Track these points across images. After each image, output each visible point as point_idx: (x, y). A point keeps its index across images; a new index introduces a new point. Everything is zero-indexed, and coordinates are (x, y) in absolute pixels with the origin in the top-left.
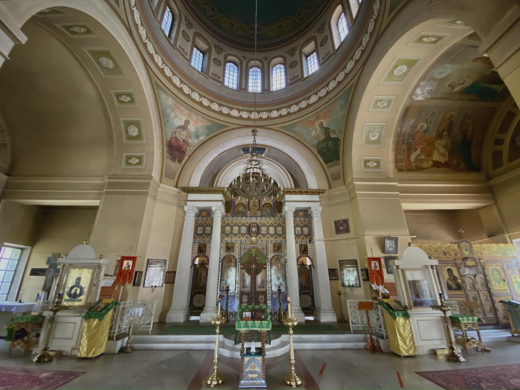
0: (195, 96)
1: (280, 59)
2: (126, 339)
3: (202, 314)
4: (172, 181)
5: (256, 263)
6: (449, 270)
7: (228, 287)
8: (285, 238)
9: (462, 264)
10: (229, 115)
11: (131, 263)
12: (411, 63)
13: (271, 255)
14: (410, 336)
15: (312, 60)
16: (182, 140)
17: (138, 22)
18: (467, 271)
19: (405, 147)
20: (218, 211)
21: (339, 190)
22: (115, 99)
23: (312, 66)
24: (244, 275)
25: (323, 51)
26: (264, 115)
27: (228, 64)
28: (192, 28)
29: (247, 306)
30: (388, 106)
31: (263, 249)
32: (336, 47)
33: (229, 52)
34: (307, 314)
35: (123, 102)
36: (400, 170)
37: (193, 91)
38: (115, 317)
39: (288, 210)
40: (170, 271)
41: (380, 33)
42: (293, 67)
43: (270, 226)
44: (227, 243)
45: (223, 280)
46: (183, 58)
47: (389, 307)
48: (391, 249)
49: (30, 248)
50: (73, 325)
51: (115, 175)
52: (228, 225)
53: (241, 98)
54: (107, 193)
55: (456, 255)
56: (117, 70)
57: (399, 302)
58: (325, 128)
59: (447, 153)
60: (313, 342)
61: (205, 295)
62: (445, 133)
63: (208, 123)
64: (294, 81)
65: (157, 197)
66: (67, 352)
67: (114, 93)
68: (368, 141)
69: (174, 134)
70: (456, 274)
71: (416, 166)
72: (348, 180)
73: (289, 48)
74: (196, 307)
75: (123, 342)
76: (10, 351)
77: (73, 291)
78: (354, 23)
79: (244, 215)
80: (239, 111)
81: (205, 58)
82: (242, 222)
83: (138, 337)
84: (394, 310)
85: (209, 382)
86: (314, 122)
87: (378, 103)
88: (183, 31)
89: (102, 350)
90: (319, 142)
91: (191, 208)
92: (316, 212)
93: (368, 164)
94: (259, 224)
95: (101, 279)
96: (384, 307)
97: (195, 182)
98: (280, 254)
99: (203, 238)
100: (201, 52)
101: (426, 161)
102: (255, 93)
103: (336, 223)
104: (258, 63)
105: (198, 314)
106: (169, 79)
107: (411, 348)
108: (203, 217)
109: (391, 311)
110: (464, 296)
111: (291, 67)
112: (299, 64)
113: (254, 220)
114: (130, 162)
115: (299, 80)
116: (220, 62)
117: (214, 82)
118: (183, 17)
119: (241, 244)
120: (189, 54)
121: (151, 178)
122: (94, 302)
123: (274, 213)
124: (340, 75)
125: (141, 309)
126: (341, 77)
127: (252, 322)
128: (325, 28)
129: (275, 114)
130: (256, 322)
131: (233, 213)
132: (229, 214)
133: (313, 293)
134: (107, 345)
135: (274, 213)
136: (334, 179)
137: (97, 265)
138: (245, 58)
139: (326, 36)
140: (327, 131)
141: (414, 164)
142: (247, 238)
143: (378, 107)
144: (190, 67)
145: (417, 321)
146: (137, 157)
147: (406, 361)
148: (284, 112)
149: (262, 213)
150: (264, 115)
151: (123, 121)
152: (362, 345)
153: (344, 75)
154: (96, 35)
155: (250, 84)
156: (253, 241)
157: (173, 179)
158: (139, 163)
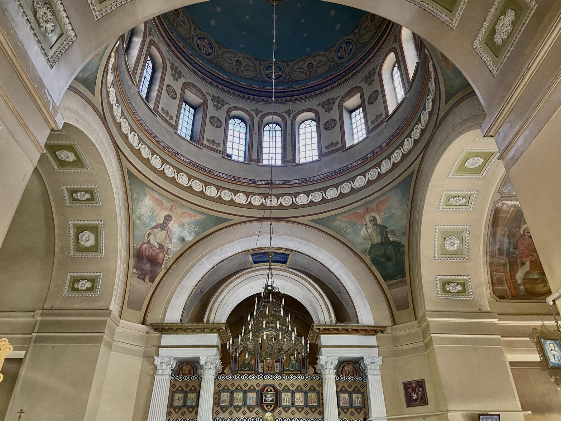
4: (138, 312)
8: (322, 413)
10: (232, 203)
12: (487, 157)
15: (358, 117)
16: (157, 246)
19: (504, 260)
21: (407, 328)
23: (357, 129)
25: (373, 110)
26: (287, 201)
27: (232, 121)
30: (467, 204)
32: (391, 111)
33: (234, 105)
35: (78, 200)
39: (326, 363)
42: (330, 127)
43: (297, 390)
46: (164, 124)
51: (51, 309)
56: (79, 163)
63: (199, 217)
64: (331, 149)
67: (67, 189)
68: (445, 253)
69: (146, 237)
71: (526, 290)
72: (420, 314)
73: (324, 98)
78: (411, 86)
79: (253, 371)
81: (197, 117)
86: (362, 216)
91: (166, 360)
97: (174, 315)
100: (191, 106)
101: (542, 283)
102: (272, 166)
103: (407, 386)
106: (147, 162)
108: (184, 375)
112: (338, 126)
115: (339, 149)
116: (221, 122)
117: (212, 153)
118: (168, 65)
120: (174, 119)
123: (304, 367)
124: (395, 154)
128: (374, 77)
129: (302, 200)
131: (235, 367)
135: (304, 367)
136: (399, 308)
140: (382, 229)
141: (522, 287)
144: (175, 135)
148: (317, 197)
149: (283, 366)
150: (287, 201)
151: (74, 225)
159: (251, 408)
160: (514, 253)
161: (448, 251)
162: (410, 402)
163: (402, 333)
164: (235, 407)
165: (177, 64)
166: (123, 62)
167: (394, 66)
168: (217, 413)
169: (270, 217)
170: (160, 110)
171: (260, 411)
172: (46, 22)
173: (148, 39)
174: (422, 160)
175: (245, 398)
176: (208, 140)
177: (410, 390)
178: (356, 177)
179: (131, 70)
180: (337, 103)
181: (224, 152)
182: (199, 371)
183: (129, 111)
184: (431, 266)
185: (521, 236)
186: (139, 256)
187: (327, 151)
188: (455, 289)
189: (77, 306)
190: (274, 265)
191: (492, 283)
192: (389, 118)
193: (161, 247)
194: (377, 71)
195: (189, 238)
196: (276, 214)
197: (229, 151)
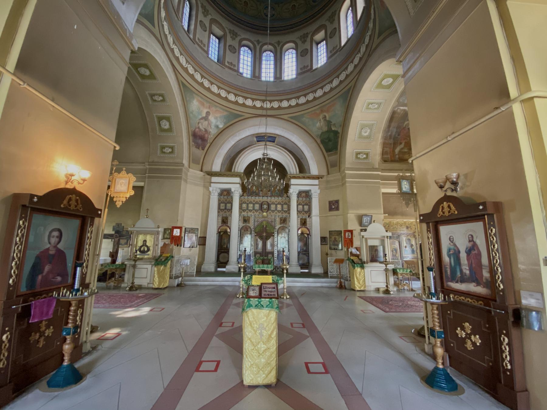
1: (292, 45)
2: (180, 279)
3: (227, 267)
5: (266, 232)
8: (289, 213)
10: (244, 105)
11: (179, 230)
19: (391, 141)
20: (236, 192)
22: (149, 98)
23: (321, 57)
24: (257, 240)
26: (276, 105)
27: (242, 49)
32: (343, 44)
33: (243, 37)
34: (302, 268)
36: (385, 161)
37: (212, 83)
42: (305, 54)
44: (244, 217)
48: (366, 224)
51: (153, 162)
52: (245, 203)
53: (254, 88)
56: (152, 76)
57: (361, 260)
61: (228, 254)
64: (304, 70)
65: (188, 180)
68: (361, 136)
71: (399, 158)
72: (342, 169)
77: (142, 249)
79: (257, 195)
80: (253, 100)
81: (220, 45)
82: (256, 200)
83: (186, 278)
88: (201, 21)
89: (167, 285)
90: (322, 133)
92: (315, 194)
93: (359, 156)
100: (217, 37)
103: (330, 203)
104: (270, 47)
105: (224, 267)
106: (192, 76)
115: (307, 71)
116: (235, 49)
117: (230, 71)
118: (200, 5)
120: (206, 46)
124: (342, 75)
125: (189, 261)
128: (335, 18)
129: (285, 104)
132: (245, 194)
134: (169, 281)
139: (335, 28)
141: (397, 156)
142: (260, 213)
144: (208, 59)
150: (276, 105)
151: (156, 116)
152: (334, 285)
157: (199, 164)
159: (256, 211)
167: (349, 9)
168: (241, 212)
169: (265, 114)
170: (197, 40)
175: (254, 207)
180: (310, 36)
181: (238, 71)
183: (178, 40)
184: (352, 144)
189: (166, 161)
190: (268, 143)
195: (221, 126)
196: (270, 113)
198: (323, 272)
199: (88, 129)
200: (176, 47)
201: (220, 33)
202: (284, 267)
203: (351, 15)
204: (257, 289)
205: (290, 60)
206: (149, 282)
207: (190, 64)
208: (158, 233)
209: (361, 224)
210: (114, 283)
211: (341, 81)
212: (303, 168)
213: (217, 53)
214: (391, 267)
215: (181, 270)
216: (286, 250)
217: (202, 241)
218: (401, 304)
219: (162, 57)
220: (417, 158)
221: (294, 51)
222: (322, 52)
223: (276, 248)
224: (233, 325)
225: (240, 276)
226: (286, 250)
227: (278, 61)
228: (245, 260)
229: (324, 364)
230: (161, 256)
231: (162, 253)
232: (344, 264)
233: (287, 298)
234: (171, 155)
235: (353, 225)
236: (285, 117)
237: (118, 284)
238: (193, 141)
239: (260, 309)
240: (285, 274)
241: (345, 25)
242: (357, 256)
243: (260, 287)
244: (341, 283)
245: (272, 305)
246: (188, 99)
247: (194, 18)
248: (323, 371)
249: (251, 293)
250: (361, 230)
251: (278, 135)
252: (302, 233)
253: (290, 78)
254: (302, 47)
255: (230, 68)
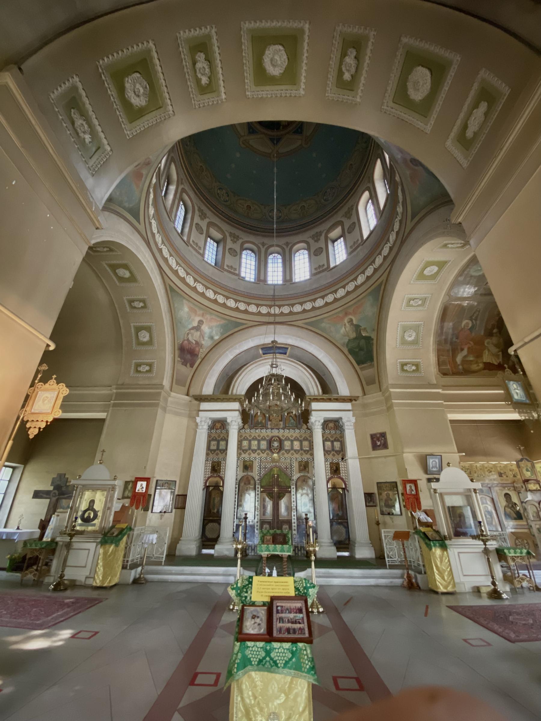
0: (210, 294)
2: (140, 569)
3: (217, 547)
4: (183, 388)
5: (279, 486)
6: (507, 496)
7: (246, 514)
8: (312, 455)
9: (522, 487)
11: (144, 484)
12: (441, 265)
13: (296, 476)
14: (449, 570)
15: (339, 246)
16: (194, 342)
17: (155, 231)
18: (530, 497)
19: (448, 347)
20: (234, 423)
21: (374, 397)
23: (339, 253)
24: (264, 500)
28: (205, 218)
29: (268, 531)
30: (423, 305)
31: (286, 468)
32: (365, 237)
33: (246, 239)
34: (339, 550)
35: (135, 308)
38: (129, 544)
39: (315, 421)
40: (180, 494)
41: (406, 234)
42: (318, 253)
45: (241, 506)
46: (194, 252)
47: (425, 536)
48: (434, 469)
49: (23, 466)
50: (87, 551)
51: (122, 385)
52: (245, 439)
53: (260, 293)
54: (115, 405)
55: (514, 476)
56: (133, 279)
57: (438, 532)
58: (356, 325)
59: (500, 353)
60: (342, 578)
61: (220, 524)
62: (495, 331)
63: (223, 322)
64: (319, 270)
66: (81, 581)
68: (404, 342)
70: (515, 499)
71: (463, 369)
72: (384, 387)
74: (209, 539)
75: (136, 571)
76: (22, 580)
77: (86, 515)
80: (258, 306)
81: (219, 249)
84: (429, 540)
85: (231, 607)
87: (412, 302)
89: (116, 580)
91: (204, 419)
92: (348, 423)
93: (405, 368)
94: (282, 438)
95: (114, 503)
96: (421, 537)
98: (306, 474)
99: (217, 454)
100: (214, 241)
103: (373, 437)
105: (213, 547)
106: (183, 280)
107: (449, 583)
108: (217, 429)
109: (427, 541)
110: (527, 527)
111: (316, 255)
113: (275, 432)
114: (139, 369)
116: (237, 252)
117: (230, 275)
118: (196, 208)
119: (261, 462)
120: (202, 249)
121: (161, 386)
122: (107, 527)
124: (369, 269)
126: (369, 271)
127: (273, 546)
129: (298, 308)
130: (277, 546)
132: (246, 426)
133: (347, 523)
136: (368, 384)
137: (110, 487)
138: (263, 244)
141: (461, 367)
142: (268, 454)
143: (412, 306)
144: (204, 262)
145: (459, 553)
146: (147, 364)
147: (444, 598)
149: (285, 424)
151: (134, 326)
152: (399, 581)
153: (373, 270)
154: (116, 251)
155: (270, 274)
156: (274, 459)
157: (184, 386)
158: (149, 371)
159: (263, 451)
160: (455, 342)
161: (407, 341)
162: (375, 447)
163: (370, 401)
164: (253, 451)
165: (203, 208)
166: (161, 201)
167: (368, 202)
168: (240, 454)
169: (274, 321)
170: (191, 242)
171: (270, 453)
172: (84, 132)
173: (181, 187)
174: (389, 272)
176: (228, 266)
177: (375, 439)
178: (338, 289)
179: (168, 210)
180: (323, 235)
181: (239, 275)
182: (227, 427)
183: (167, 240)
184: (393, 351)
185: (462, 329)
186: (182, 349)
187: (316, 272)
188: (411, 370)
189: (141, 383)
190: (278, 355)
191: (438, 364)
192: (364, 242)
193: (197, 343)
194: (354, 208)
195: (216, 338)
196: (278, 319)
197: (243, 274)
198: (373, 556)
199: (21, 325)
200: (165, 247)
201: (219, 236)
202: (311, 549)
203: (372, 207)
204: (262, 612)
205: (302, 261)
206: (88, 574)
207: (180, 266)
208: (113, 488)
209: (426, 470)
210: (35, 575)
211: (367, 277)
212: (327, 389)
213: (214, 257)
214: (492, 545)
215: (143, 551)
216: (311, 517)
217: (180, 502)
218: (531, 621)
219: (147, 256)
220: (526, 343)
221: (306, 252)
222: (340, 249)
223: (294, 513)
224: (216, 683)
225: (236, 566)
226: (311, 517)
227: (288, 263)
228: (245, 534)
229: (358, 680)
230: (113, 527)
231: (116, 521)
232: (410, 541)
233: (318, 612)
234: (149, 375)
235: (415, 472)
236: (299, 323)
237: (39, 577)
238: (180, 356)
239: (269, 670)
240: (313, 563)
241: (366, 220)
242: (427, 525)
243: (270, 606)
244: (409, 576)
245: (299, 659)
246: (176, 305)
247: (189, 221)
248: (357, 687)
249: (251, 627)
250: (429, 480)
251: (291, 345)
252: (334, 488)
253: (303, 279)
254: (315, 246)
255: (230, 272)
